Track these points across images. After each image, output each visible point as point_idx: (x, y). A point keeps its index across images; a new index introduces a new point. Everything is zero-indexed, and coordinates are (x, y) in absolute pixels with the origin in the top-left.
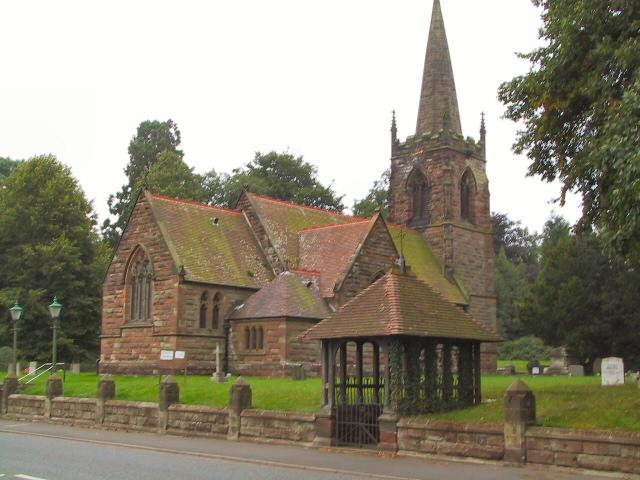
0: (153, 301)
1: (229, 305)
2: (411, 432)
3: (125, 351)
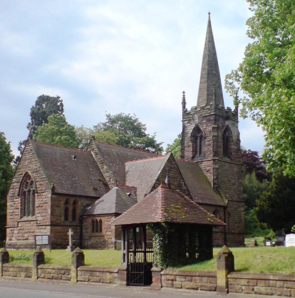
0: (36, 205)
1: (83, 207)
2: (168, 277)
3: (20, 235)
